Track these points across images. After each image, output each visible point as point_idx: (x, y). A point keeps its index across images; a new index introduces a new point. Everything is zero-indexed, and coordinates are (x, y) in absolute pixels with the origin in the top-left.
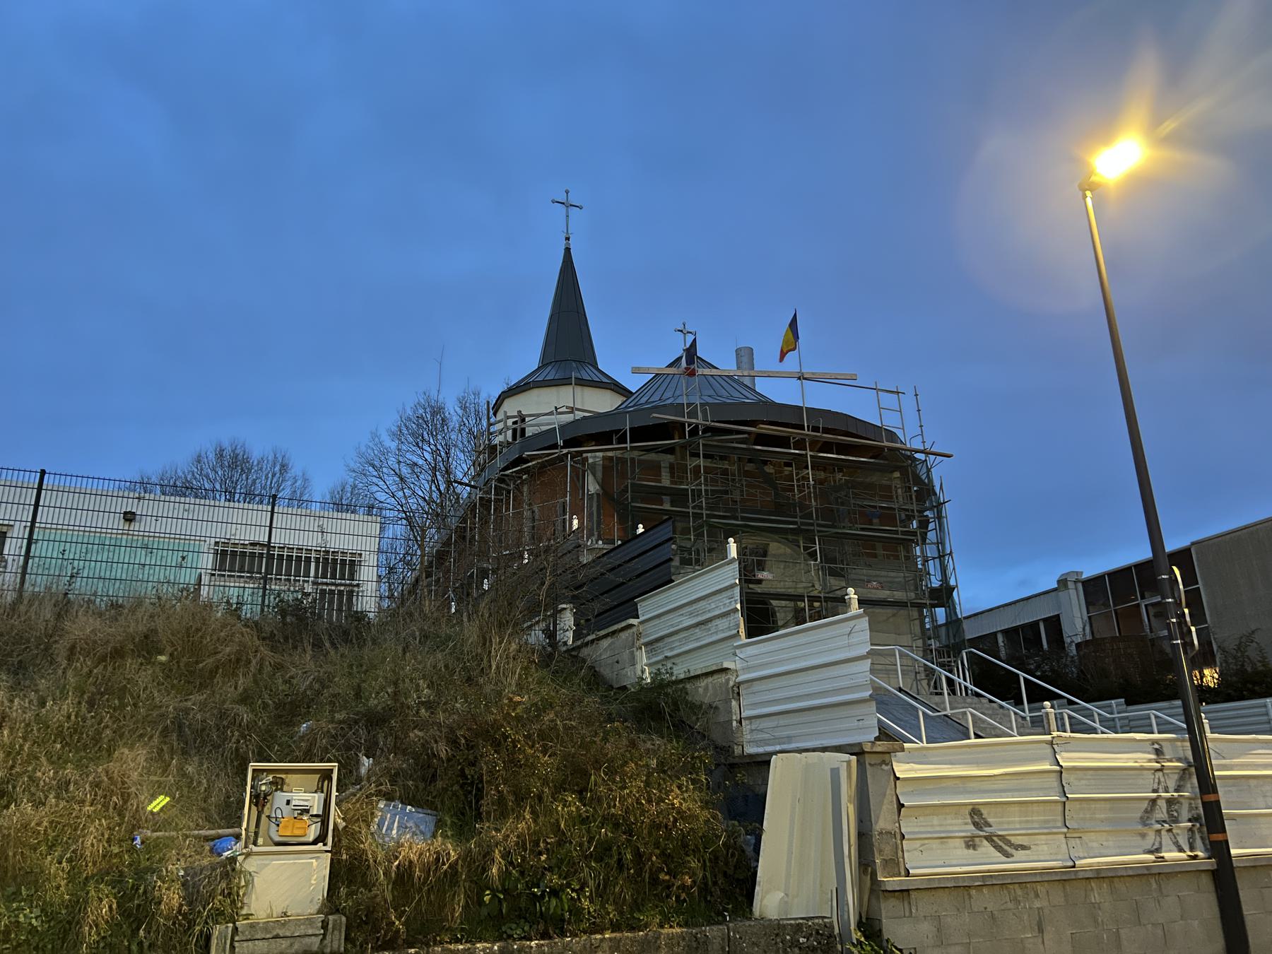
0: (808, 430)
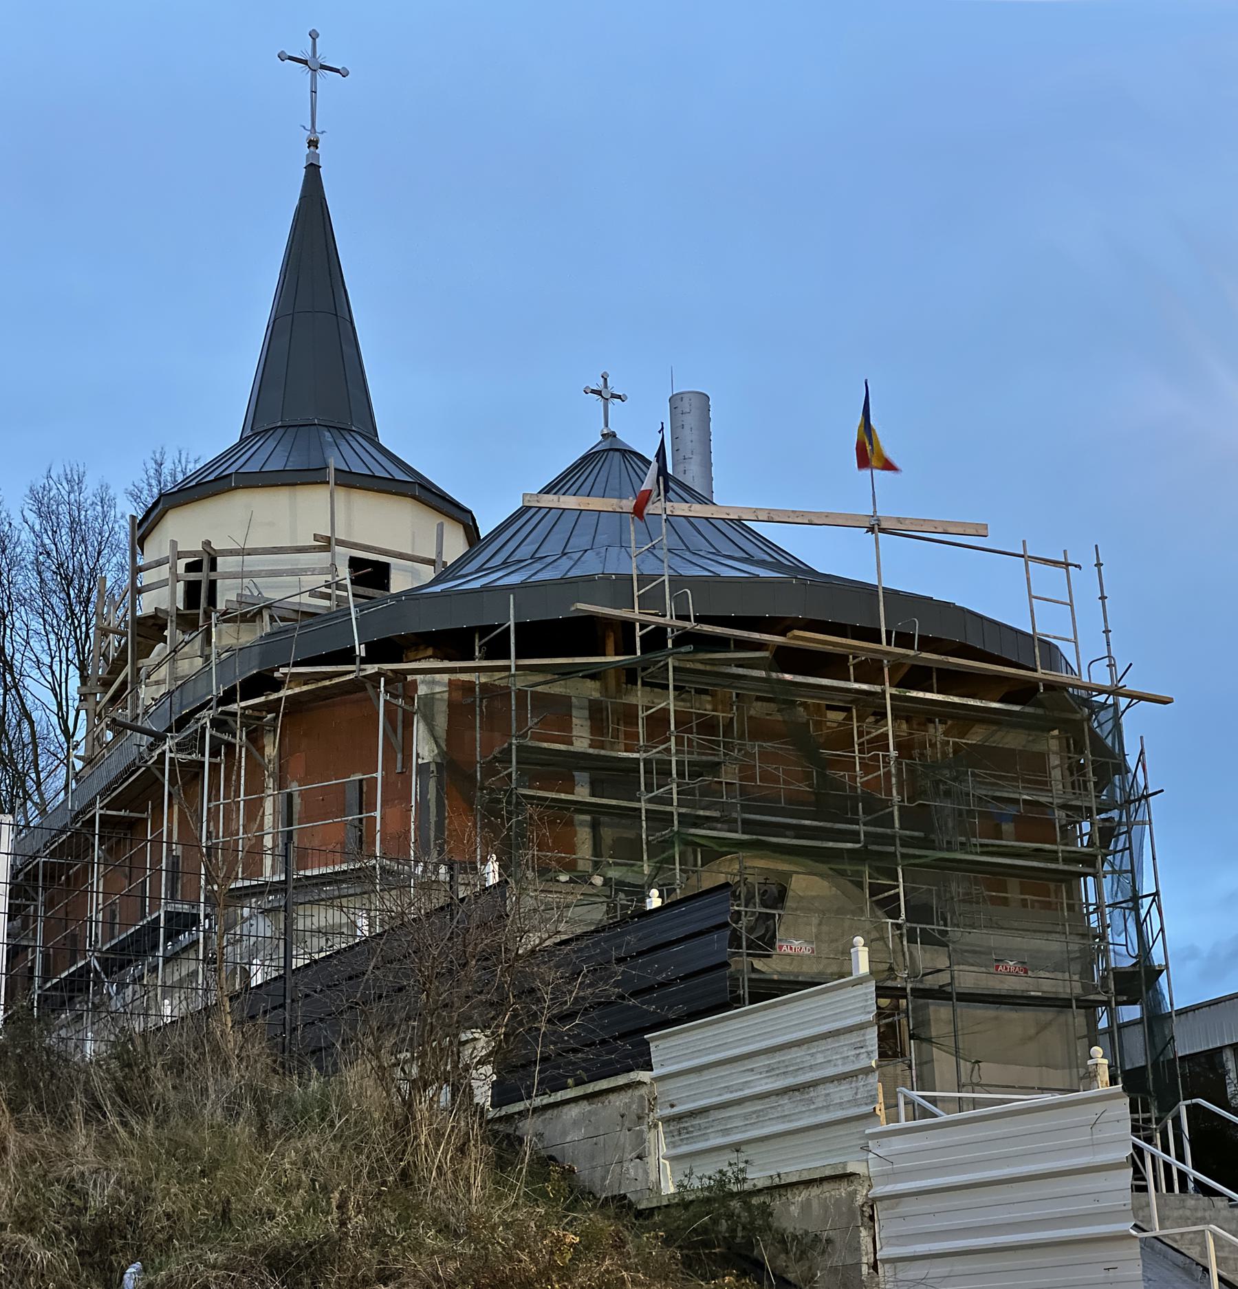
0: (889, 643)
